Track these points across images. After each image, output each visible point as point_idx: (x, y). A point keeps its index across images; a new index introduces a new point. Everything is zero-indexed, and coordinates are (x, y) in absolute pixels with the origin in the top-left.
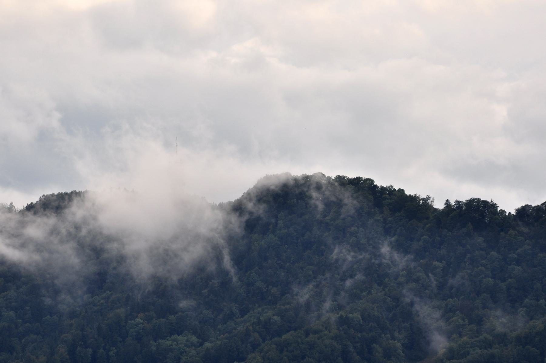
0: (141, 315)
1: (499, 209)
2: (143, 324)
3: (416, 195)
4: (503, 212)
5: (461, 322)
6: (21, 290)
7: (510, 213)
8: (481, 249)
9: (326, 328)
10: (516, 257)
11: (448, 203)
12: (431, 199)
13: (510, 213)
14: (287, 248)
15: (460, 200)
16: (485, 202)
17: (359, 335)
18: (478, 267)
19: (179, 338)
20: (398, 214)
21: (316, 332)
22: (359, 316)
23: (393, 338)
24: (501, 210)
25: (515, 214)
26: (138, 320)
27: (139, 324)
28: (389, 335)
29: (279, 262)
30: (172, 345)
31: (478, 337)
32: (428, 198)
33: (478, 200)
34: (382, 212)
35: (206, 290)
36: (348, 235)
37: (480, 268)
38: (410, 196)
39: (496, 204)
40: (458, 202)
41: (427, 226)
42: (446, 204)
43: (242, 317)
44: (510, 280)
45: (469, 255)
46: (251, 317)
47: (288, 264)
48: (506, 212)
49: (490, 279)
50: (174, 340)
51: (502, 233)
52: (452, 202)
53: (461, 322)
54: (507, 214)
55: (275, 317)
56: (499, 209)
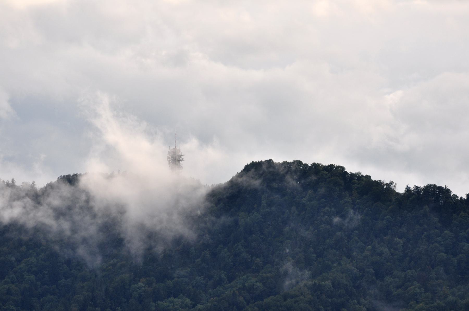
0: (143, 280)
1: (452, 194)
2: (144, 287)
3: (381, 180)
4: (456, 196)
5: (418, 290)
6: (41, 256)
7: (461, 198)
8: (436, 228)
9: (302, 294)
10: (466, 235)
11: (408, 188)
12: (394, 184)
13: (461, 198)
14: (269, 225)
15: (419, 186)
16: (440, 188)
17: (330, 300)
18: (433, 243)
19: (175, 300)
20: (365, 197)
21: (292, 297)
22: (330, 284)
23: (359, 303)
24: (454, 195)
25: (466, 198)
26: (140, 284)
27: (141, 288)
28: (355, 301)
29: (262, 236)
30: (169, 306)
31: (432, 303)
32: (391, 183)
33: (435, 186)
34: (351, 195)
35: (199, 260)
36: (322, 214)
37: (435, 244)
38: (375, 181)
39: (449, 190)
40: (417, 187)
41: (390, 207)
42: (406, 189)
43: (230, 283)
44: (460, 255)
45: (425, 233)
46: (237, 283)
47: (270, 238)
48: (458, 197)
49: (444, 254)
50: (171, 302)
51: (454, 215)
52: (412, 187)
53: (418, 290)
54: (459, 198)
55: (258, 284)
56: (452, 194)
